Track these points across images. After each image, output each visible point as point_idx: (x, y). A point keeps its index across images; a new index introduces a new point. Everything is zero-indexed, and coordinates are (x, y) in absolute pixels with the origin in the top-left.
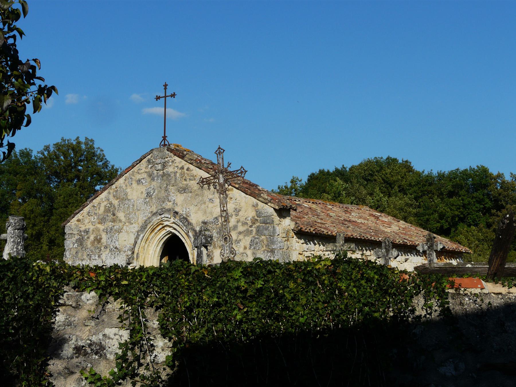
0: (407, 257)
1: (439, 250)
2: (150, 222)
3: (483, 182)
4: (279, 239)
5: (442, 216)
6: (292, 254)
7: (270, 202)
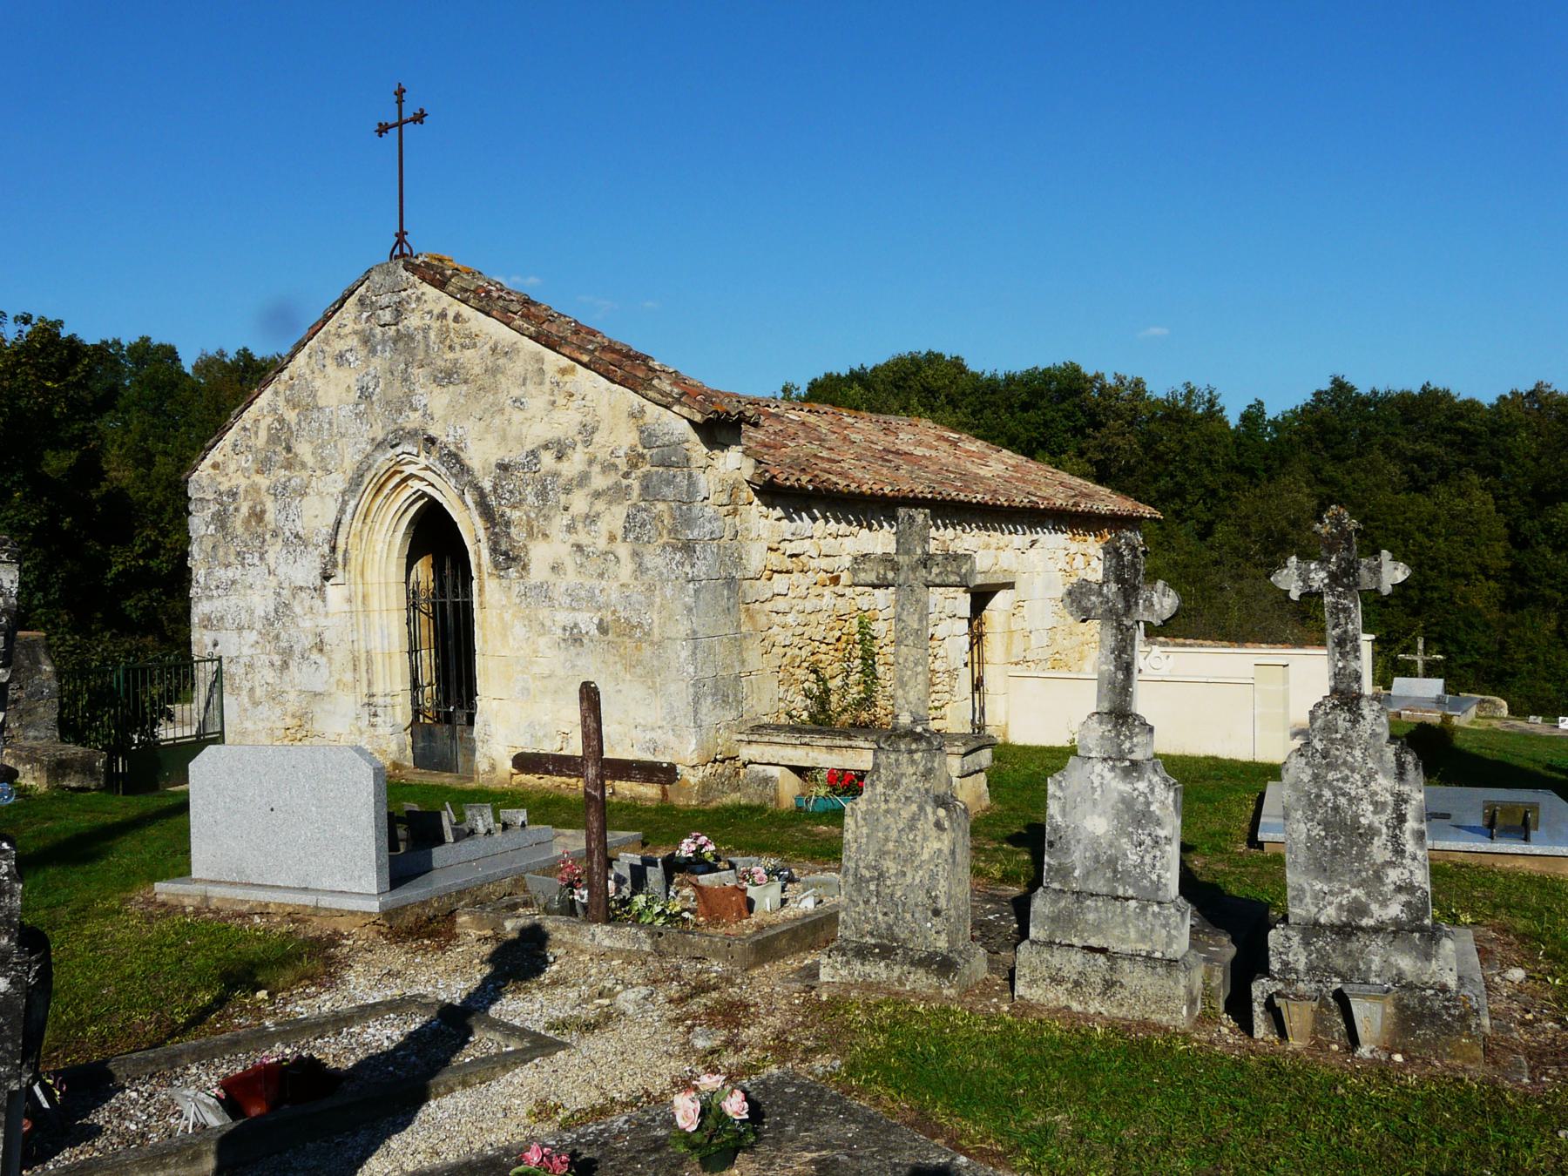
1: (1386, 589)
2: (369, 468)
3: (1075, 386)
4: (709, 512)
6: (748, 552)
7: (678, 401)
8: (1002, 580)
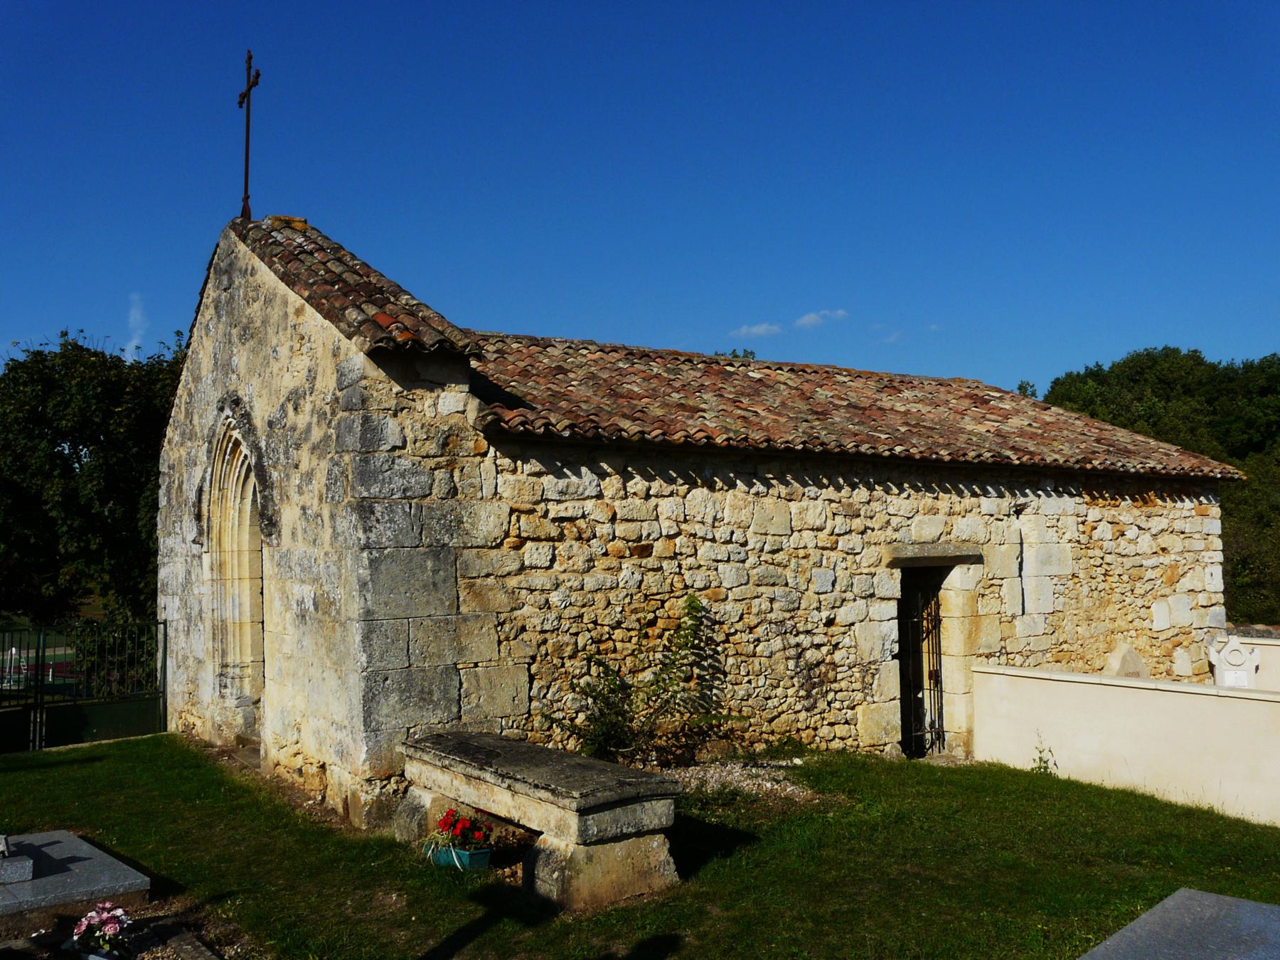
0: (1022, 500)
5: (1250, 424)
8: (966, 550)
